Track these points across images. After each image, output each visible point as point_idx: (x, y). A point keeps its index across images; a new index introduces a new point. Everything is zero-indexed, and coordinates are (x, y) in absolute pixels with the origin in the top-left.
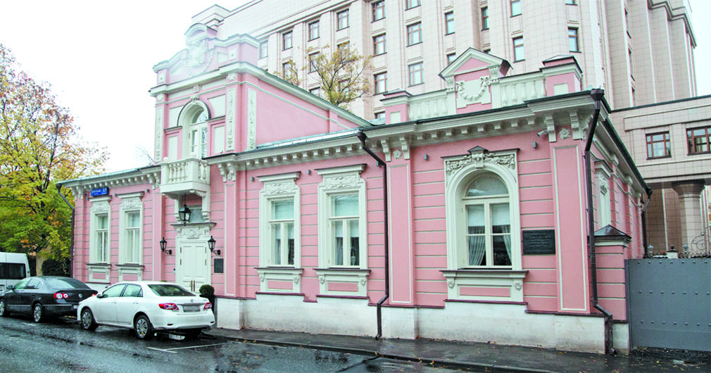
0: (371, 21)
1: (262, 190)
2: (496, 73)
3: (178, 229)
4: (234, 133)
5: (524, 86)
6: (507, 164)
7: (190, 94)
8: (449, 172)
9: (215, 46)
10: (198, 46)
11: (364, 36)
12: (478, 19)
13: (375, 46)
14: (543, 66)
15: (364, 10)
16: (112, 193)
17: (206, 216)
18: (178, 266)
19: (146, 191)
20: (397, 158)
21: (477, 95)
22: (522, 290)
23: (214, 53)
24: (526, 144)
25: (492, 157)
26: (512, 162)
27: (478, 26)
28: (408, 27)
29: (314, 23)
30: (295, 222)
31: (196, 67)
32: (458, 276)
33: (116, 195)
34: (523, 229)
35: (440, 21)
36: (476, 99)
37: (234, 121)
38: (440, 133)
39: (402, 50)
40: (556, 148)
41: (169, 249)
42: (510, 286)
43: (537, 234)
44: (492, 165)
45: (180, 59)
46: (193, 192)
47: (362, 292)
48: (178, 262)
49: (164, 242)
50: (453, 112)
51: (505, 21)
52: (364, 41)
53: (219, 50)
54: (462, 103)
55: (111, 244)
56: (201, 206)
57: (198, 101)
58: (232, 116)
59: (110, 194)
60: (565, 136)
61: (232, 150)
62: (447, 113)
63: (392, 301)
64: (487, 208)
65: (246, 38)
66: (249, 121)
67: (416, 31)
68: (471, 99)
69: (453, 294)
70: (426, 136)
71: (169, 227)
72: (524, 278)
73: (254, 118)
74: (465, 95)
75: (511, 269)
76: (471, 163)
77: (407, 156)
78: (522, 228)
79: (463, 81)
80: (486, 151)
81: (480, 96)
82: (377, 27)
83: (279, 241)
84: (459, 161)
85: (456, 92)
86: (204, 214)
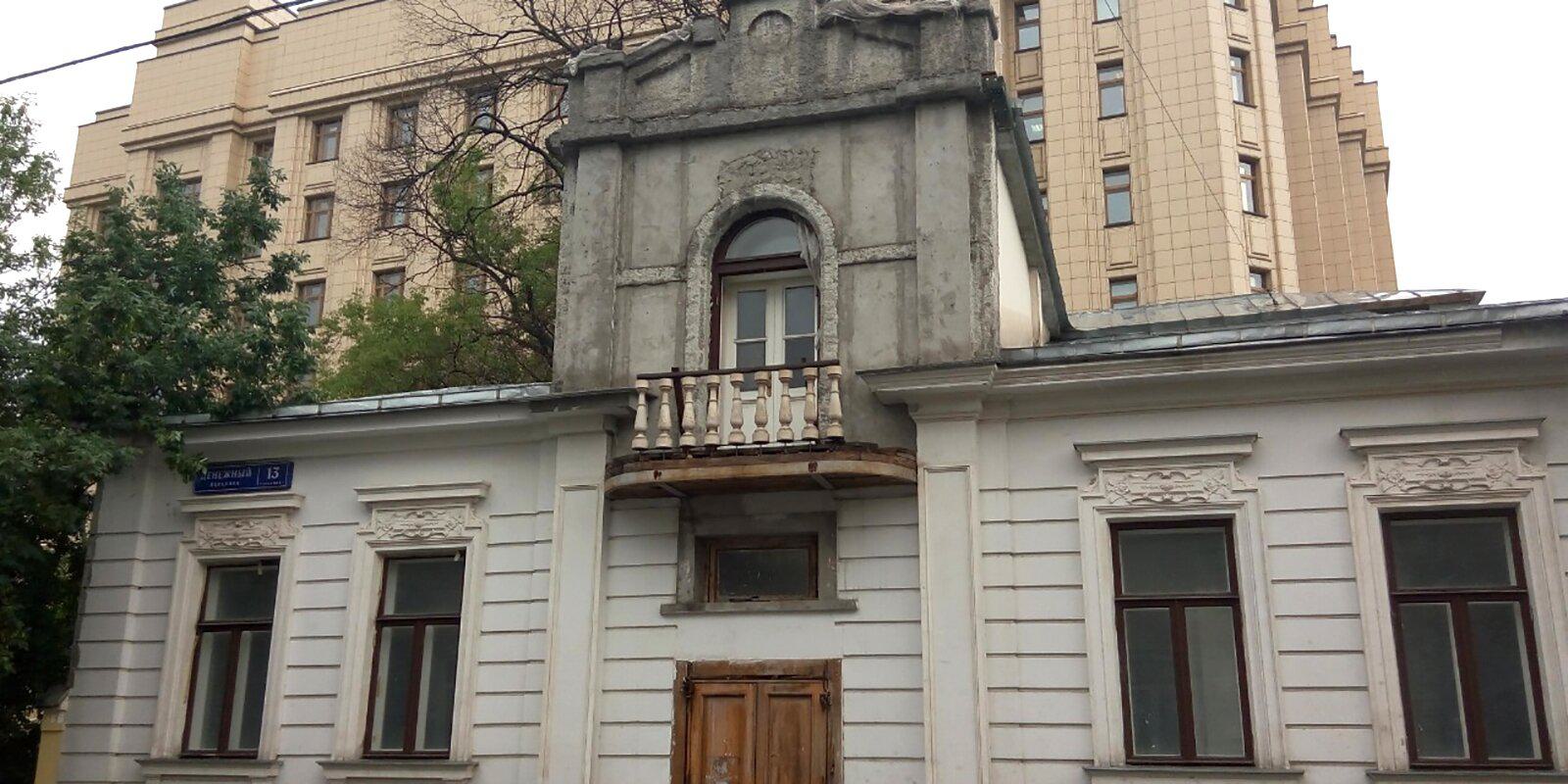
15: (234, 153)
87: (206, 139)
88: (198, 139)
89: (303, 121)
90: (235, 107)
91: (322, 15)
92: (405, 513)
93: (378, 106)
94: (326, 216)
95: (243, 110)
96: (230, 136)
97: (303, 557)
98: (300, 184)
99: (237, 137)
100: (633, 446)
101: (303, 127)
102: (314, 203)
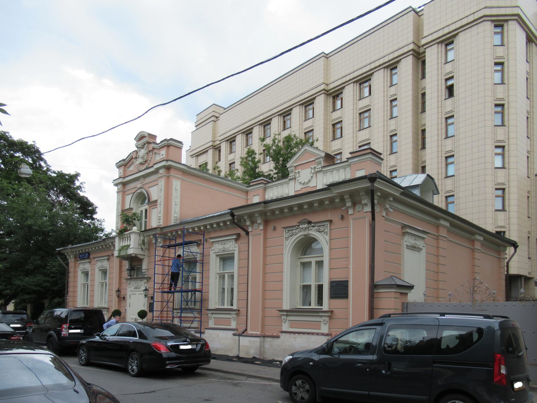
0: (331, 110)
1: (212, 249)
2: (320, 163)
3: (129, 282)
4: (162, 212)
5: (345, 170)
6: (323, 231)
7: (138, 184)
8: (287, 239)
9: (153, 148)
10: (142, 148)
11: (325, 124)
12: (417, 104)
13: (334, 132)
14: (350, 156)
15: (326, 102)
16: (91, 257)
17: (145, 272)
18: (128, 308)
19: (111, 255)
20: (256, 229)
21: (307, 181)
22: (327, 325)
23: (153, 154)
24: (335, 217)
25: (313, 226)
26: (326, 230)
27: (418, 109)
28: (360, 114)
29: (287, 115)
30: (234, 273)
31: (141, 164)
32: (288, 314)
33: (94, 258)
34: (332, 280)
35: (386, 107)
36: (307, 183)
37: (162, 204)
38: (281, 210)
39: (355, 133)
40: (353, 219)
41: (122, 296)
42: (321, 322)
43: (339, 283)
44: (313, 233)
45: (132, 158)
46: (134, 255)
47: (233, 325)
48: (128, 305)
49: (119, 291)
50: (292, 193)
51: (440, 103)
52: (325, 129)
53: (155, 151)
54: (299, 187)
55: (238, 281)
56: (142, 265)
57: (142, 190)
58: (161, 201)
59: (90, 258)
60: (359, 210)
61: (161, 225)
62: (288, 194)
63: (249, 332)
64: (313, 264)
65: (171, 142)
66: (173, 204)
67: (366, 117)
68: (304, 184)
69: (286, 327)
70: (273, 211)
71: (124, 281)
72: (330, 316)
73: (178, 201)
74: (300, 181)
75: (322, 309)
76: (300, 231)
77: (261, 227)
78: (330, 279)
79: (300, 170)
80: (310, 223)
81: (309, 181)
82: (336, 115)
83: (224, 289)
84: (293, 230)
85: (295, 179)
86: (143, 271)
87: (207, 151)
88: (205, 152)
89: (260, 126)
90: (324, 83)
91: (343, 50)
92: (220, 244)
93: (386, 70)
94: (368, 118)
95: (214, 142)
96: (323, 95)
97: (445, 264)
98: (356, 109)
99: (214, 150)
100: (365, 211)
101: (440, 48)
102: (307, 134)
